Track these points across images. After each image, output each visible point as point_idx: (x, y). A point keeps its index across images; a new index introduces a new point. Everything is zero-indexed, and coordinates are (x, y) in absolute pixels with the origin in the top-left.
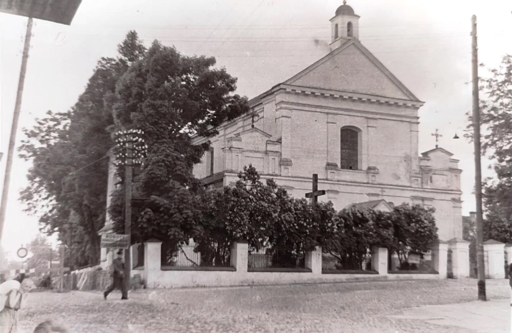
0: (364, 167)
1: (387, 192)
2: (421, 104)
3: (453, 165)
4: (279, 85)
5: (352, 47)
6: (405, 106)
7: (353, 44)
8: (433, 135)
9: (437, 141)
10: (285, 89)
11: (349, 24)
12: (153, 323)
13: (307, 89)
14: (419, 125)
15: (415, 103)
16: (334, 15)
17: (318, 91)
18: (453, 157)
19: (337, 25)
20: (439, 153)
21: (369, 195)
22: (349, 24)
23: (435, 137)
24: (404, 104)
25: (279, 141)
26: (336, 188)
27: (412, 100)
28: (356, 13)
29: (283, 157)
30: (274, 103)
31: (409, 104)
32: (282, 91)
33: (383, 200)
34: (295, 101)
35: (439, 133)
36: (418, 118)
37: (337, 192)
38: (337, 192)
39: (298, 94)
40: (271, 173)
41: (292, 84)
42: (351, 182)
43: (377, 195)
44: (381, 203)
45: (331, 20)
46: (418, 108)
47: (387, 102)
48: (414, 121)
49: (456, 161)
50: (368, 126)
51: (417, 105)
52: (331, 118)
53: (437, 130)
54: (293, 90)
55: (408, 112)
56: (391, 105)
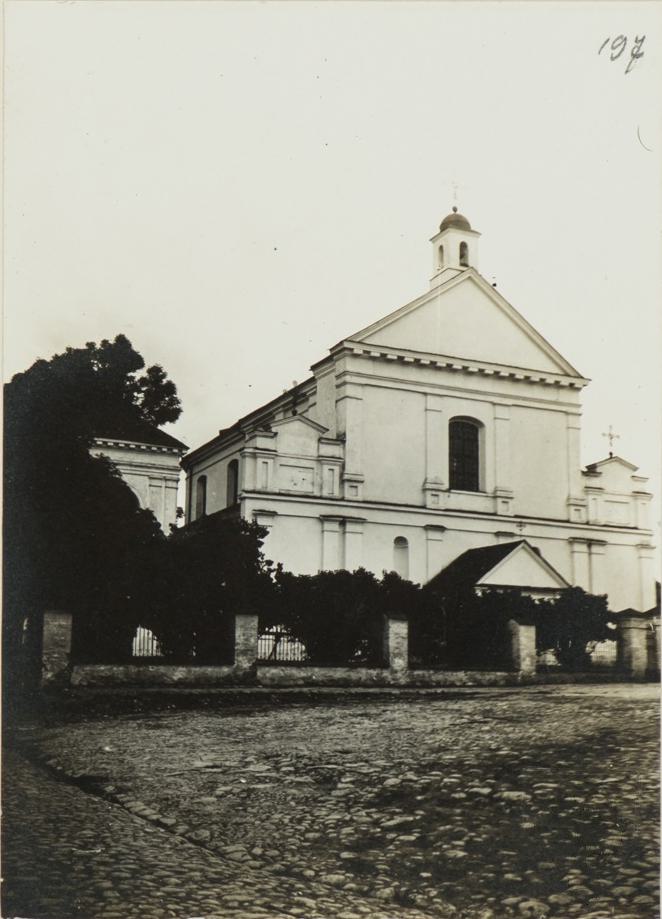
0: (489, 489)
1: (528, 530)
2: (585, 382)
3: (639, 487)
4: (341, 343)
5: (469, 284)
6: (557, 385)
7: (469, 277)
8: (604, 435)
9: (611, 444)
10: (352, 350)
11: (463, 246)
12: (630, 792)
13: (408, 353)
14: (581, 418)
15: (573, 381)
16: (439, 231)
17: (412, 355)
18: (636, 474)
19: (441, 248)
20: (615, 466)
21: (498, 534)
22: (463, 246)
23: (607, 438)
24: (383, 356)
25: (341, 439)
26: (363, 514)
27: (567, 375)
28: (472, 228)
29: (349, 469)
30: (333, 375)
31: (565, 381)
32: (346, 352)
33: (524, 541)
34: (370, 372)
35: (613, 432)
36: (579, 406)
37: (273, 514)
38: (441, 529)
39: (374, 359)
40: (259, 487)
41: (367, 342)
42: (280, 494)
43: (511, 535)
44: (520, 546)
45: (433, 240)
46: (579, 389)
47: (542, 380)
48: (571, 412)
49: (644, 479)
50: (495, 418)
51: (578, 383)
52: (432, 402)
53: (611, 427)
54: (365, 352)
55: (565, 396)
56: (472, 374)
